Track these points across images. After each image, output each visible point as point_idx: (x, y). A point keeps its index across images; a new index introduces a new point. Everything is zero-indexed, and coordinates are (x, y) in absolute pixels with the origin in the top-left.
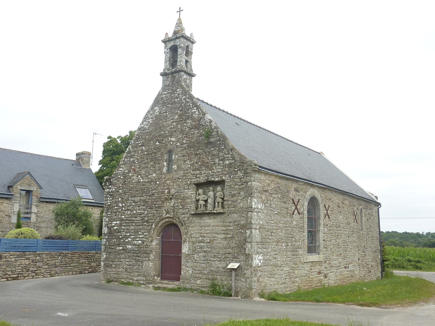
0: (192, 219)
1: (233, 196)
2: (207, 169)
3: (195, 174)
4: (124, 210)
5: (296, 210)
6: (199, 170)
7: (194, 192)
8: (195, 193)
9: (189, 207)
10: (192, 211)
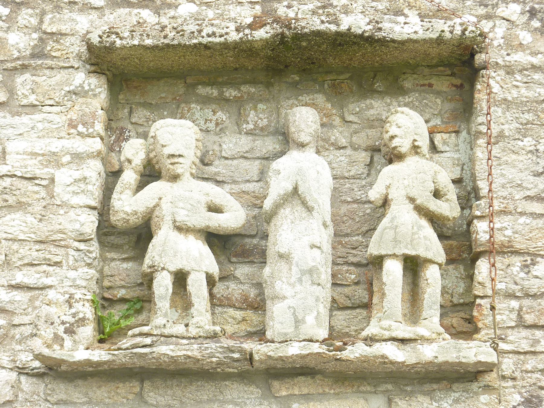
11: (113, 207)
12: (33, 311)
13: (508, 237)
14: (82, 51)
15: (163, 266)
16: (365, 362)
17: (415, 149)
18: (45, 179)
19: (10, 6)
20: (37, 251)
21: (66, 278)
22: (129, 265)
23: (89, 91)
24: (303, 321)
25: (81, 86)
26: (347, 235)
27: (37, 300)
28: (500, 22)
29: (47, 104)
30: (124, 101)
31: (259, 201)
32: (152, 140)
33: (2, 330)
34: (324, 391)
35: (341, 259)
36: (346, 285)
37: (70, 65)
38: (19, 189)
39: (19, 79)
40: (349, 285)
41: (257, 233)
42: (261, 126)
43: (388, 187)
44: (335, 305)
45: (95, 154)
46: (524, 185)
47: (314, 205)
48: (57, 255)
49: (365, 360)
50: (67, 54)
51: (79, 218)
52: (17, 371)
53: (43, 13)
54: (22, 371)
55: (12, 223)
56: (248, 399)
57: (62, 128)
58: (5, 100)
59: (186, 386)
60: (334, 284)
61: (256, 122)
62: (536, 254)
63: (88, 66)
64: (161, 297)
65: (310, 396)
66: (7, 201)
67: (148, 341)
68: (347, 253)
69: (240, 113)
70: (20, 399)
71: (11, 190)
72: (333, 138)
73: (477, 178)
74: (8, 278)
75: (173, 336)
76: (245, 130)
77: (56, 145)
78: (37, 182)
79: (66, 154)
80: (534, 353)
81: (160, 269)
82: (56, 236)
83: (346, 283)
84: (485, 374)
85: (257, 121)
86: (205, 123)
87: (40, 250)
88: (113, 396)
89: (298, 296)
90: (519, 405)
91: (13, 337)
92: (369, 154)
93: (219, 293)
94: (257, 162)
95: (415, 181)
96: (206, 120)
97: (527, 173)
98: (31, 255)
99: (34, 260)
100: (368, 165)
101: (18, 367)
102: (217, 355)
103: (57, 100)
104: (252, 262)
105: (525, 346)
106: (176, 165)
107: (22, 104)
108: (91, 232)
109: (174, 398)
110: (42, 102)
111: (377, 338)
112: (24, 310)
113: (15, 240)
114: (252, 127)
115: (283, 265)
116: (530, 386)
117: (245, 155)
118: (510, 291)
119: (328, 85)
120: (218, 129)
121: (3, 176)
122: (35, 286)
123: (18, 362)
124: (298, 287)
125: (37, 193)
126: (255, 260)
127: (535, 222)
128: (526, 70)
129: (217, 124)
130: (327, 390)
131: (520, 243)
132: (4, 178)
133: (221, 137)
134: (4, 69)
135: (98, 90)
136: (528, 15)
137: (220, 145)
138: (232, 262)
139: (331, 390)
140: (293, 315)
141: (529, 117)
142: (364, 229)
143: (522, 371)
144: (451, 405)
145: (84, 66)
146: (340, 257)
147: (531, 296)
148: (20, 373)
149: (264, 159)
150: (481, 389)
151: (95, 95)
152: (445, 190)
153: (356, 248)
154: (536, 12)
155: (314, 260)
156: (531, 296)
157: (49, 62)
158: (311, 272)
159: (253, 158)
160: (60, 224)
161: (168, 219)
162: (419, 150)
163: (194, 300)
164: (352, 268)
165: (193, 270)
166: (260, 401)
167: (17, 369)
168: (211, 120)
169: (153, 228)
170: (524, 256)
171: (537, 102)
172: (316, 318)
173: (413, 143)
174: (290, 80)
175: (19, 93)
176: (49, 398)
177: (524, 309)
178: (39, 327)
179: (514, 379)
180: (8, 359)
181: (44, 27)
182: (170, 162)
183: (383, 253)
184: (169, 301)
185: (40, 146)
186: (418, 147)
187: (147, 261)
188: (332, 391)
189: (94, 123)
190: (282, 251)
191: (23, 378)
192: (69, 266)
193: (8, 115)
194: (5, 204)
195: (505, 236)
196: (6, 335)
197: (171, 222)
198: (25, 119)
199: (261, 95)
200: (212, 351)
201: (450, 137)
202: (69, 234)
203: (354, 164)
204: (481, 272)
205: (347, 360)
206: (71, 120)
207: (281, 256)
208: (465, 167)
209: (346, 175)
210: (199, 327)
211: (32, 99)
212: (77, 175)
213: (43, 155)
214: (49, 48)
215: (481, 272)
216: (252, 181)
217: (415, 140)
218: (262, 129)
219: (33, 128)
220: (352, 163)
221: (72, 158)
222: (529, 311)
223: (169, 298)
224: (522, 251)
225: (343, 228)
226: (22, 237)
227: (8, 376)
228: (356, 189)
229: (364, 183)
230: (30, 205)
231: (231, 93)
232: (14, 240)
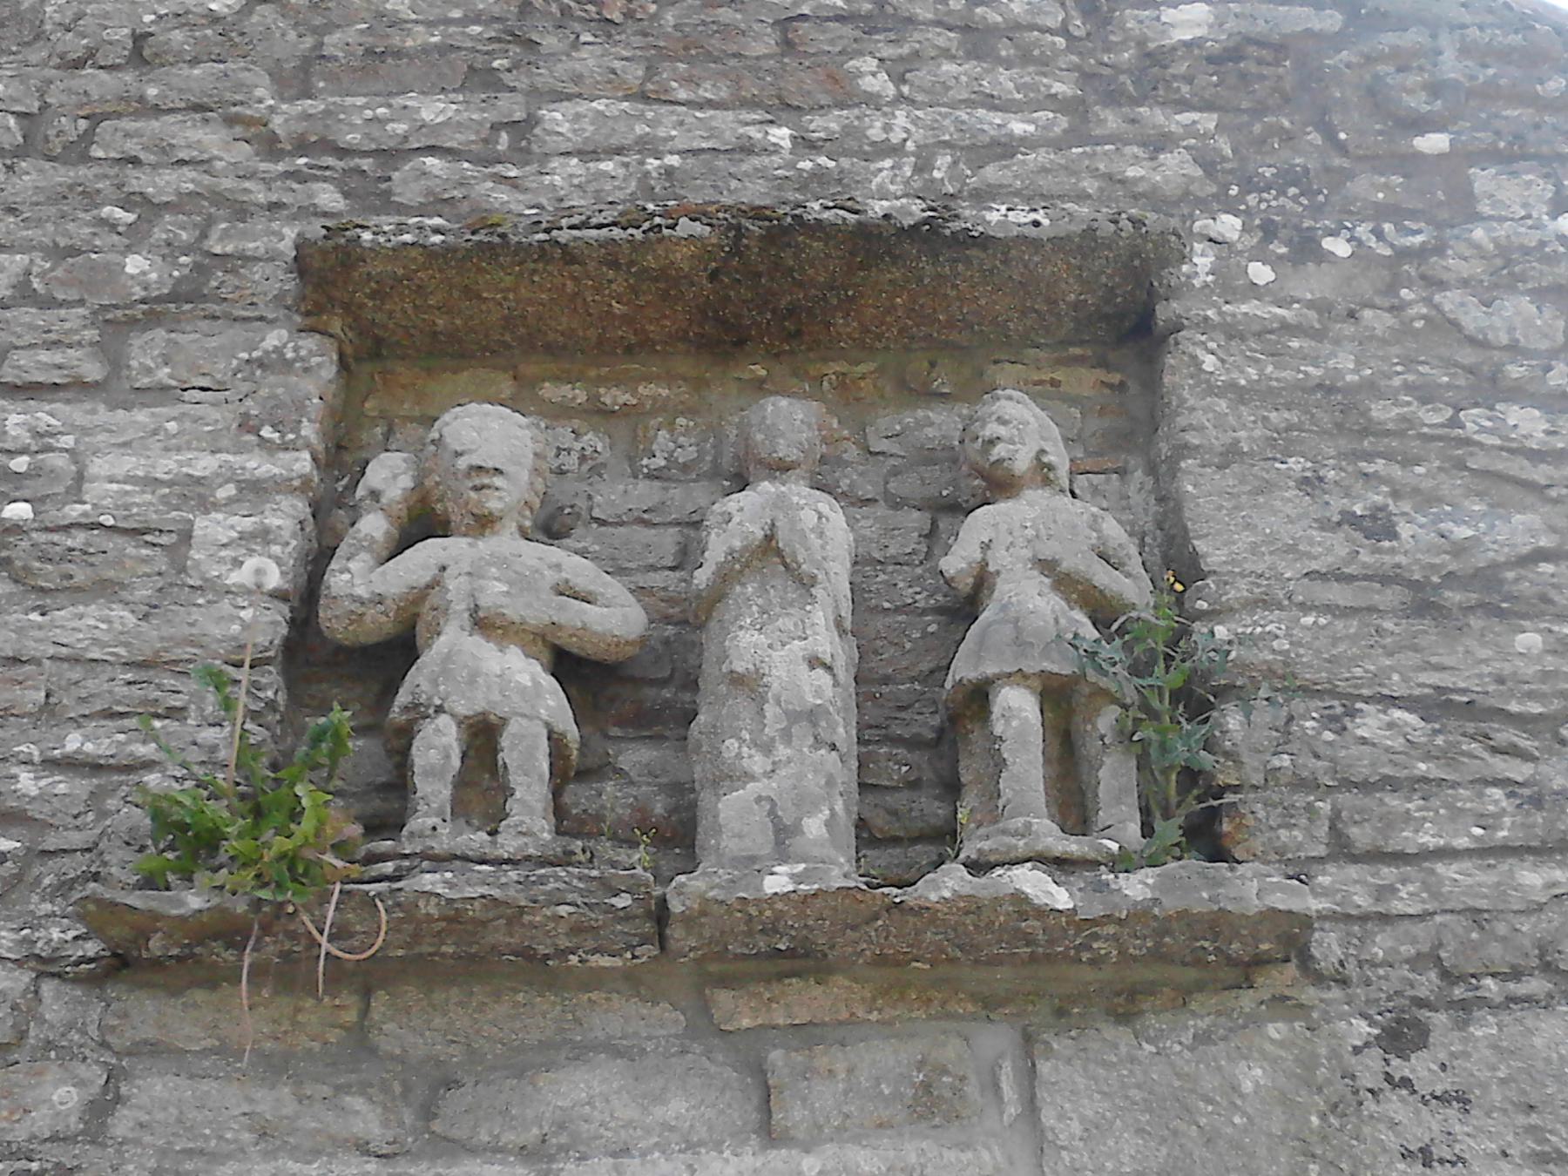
0: (101, 1109)
1: (1453, 597)
2: (690, 81)
3: (352, 138)
4: (438, 920)
5: (1477, 428)
6: (482, 80)
7: (258, 465)
8: (280, 485)
9: (61, 785)
10: (1093, 962)
11: (328, 588)
12: (96, 821)
13: (1281, 653)
14: (286, 288)
15: (438, 702)
16: (967, 913)
17: (1043, 472)
18: (171, 531)
19: (138, 210)
20: (129, 683)
21: (195, 744)
22: (358, 743)
23: (294, 360)
24: (796, 829)
25: (278, 350)
26: (886, 680)
27: (111, 797)
28: (1201, 246)
29: (195, 384)
30: (375, 414)
31: (677, 610)
32: (433, 448)
33: (8, 864)
34: (853, 1014)
35: (873, 731)
36: (886, 788)
37: (257, 314)
38: (104, 552)
39: (137, 341)
40: (895, 789)
41: (672, 676)
42: (680, 460)
43: (986, 547)
44: (865, 835)
45: (296, 483)
46: (1301, 547)
47: (816, 571)
48: (178, 692)
49: (972, 906)
50: (253, 294)
51: (242, 614)
52: (32, 969)
53: (210, 221)
54: (46, 966)
55: (76, 624)
56: (649, 1038)
57: (225, 432)
58: (98, 378)
59: (484, 1004)
60: (863, 787)
61: (671, 453)
62: (1351, 695)
63: (298, 319)
64: (430, 773)
65: (818, 1031)
66: (71, 577)
67: (388, 868)
68: (887, 719)
69: (636, 436)
70: (32, 1041)
71: (86, 553)
72: (844, 484)
73: (1191, 535)
74: (44, 745)
75: (456, 857)
76: (645, 470)
77: (204, 465)
78: (148, 538)
79: (227, 482)
80: (1385, 918)
81: (431, 711)
82: (180, 651)
83: (886, 783)
84: (1269, 966)
85: (673, 451)
86: (558, 456)
87: (135, 683)
88: (286, 1032)
89: (783, 772)
90: (1367, 1045)
91: (38, 880)
92: (927, 515)
93: (576, 805)
94: (673, 530)
95: (1052, 526)
96: (558, 448)
97: (1305, 523)
98: (110, 692)
99: (119, 703)
100: (926, 536)
101: (38, 957)
102: (570, 897)
103: (219, 376)
104: (660, 738)
105: (1362, 901)
106: (484, 491)
107: (137, 386)
108: (267, 644)
109: (449, 1037)
110: (185, 382)
111: (992, 858)
112: (76, 817)
113: (77, 661)
114: (663, 463)
115: (741, 704)
116: (1389, 999)
117: (646, 516)
118: (1305, 774)
119: (830, 383)
120: (585, 467)
121: (72, 525)
122: (111, 761)
123: (40, 944)
124: (782, 751)
125: (146, 560)
126: (667, 733)
127: (1339, 624)
128: (1271, 332)
129: (583, 458)
130: (861, 1013)
131: (1312, 667)
132: (73, 531)
133: (590, 484)
134: (106, 321)
135: (315, 360)
136: (1260, 234)
137: (590, 497)
138: (610, 738)
139: (870, 1012)
140: (769, 815)
141: (1293, 417)
142: (925, 666)
143: (1360, 964)
144: (1191, 1049)
145: (289, 318)
146: (871, 727)
147: (1356, 785)
148: (41, 975)
149: (688, 524)
150: (1263, 1007)
151: (306, 370)
152: (1122, 553)
153: (909, 706)
154: (1277, 228)
155: (818, 692)
156: (1356, 785)
157: (216, 308)
158: (812, 716)
159: (664, 524)
160: (191, 625)
161: (460, 606)
162: (1051, 476)
163: (515, 779)
164: (901, 751)
165: (518, 714)
166: (682, 1045)
167: (32, 964)
168: (569, 451)
169: (420, 641)
170: (1322, 700)
171: (1304, 390)
172: (827, 824)
173: (1038, 458)
174: (746, 376)
175: (134, 363)
176: (109, 1038)
177: (1344, 814)
178: (107, 857)
179: (1344, 982)
180: (13, 936)
181: (206, 245)
182: (471, 485)
183: (990, 670)
184: (450, 787)
185: (166, 466)
186: (1050, 467)
187: (403, 698)
188: (874, 1016)
189: (300, 421)
190: (739, 667)
191: (48, 988)
192: (204, 718)
193: (102, 408)
194: (65, 583)
195: (1274, 651)
196: (19, 877)
197: (466, 615)
198: (141, 416)
199: (682, 402)
200: (557, 885)
201: (1108, 481)
202: (214, 646)
203: (896, 532)
204: (1227, 732)
205: (921, 908)
206: (246, 415)
207: (737, 680)
208: (1148, 540)
209: (877, 555)
210: (524, 834)
211: (163, 375)
212: (248, 524)
213: (170, 484)
214: (214, 284)
215: (1227, 732)
216: (660, 569)
217: (1043, 451)
218: (685, 468)
219: (155, 432)
220: (889, 531)
221: (240, 490)
222: (1357, 817)
223: (450, 778)
224: (1319, 687)
225: (873, 665)
226: (95, 654)
227: (7, 978)
228: (901, 585)
229: (919, 571)
230: (123, 586)
231: (614, 397)
232: (75, 660)
